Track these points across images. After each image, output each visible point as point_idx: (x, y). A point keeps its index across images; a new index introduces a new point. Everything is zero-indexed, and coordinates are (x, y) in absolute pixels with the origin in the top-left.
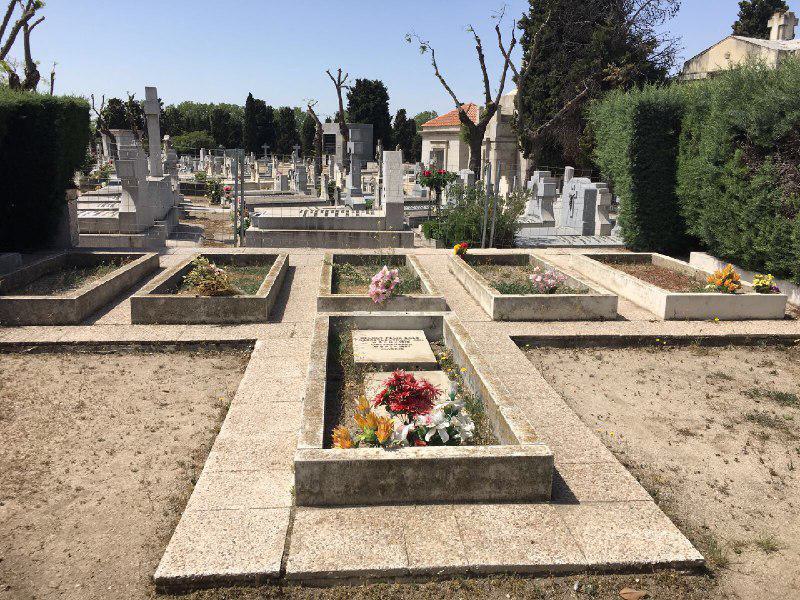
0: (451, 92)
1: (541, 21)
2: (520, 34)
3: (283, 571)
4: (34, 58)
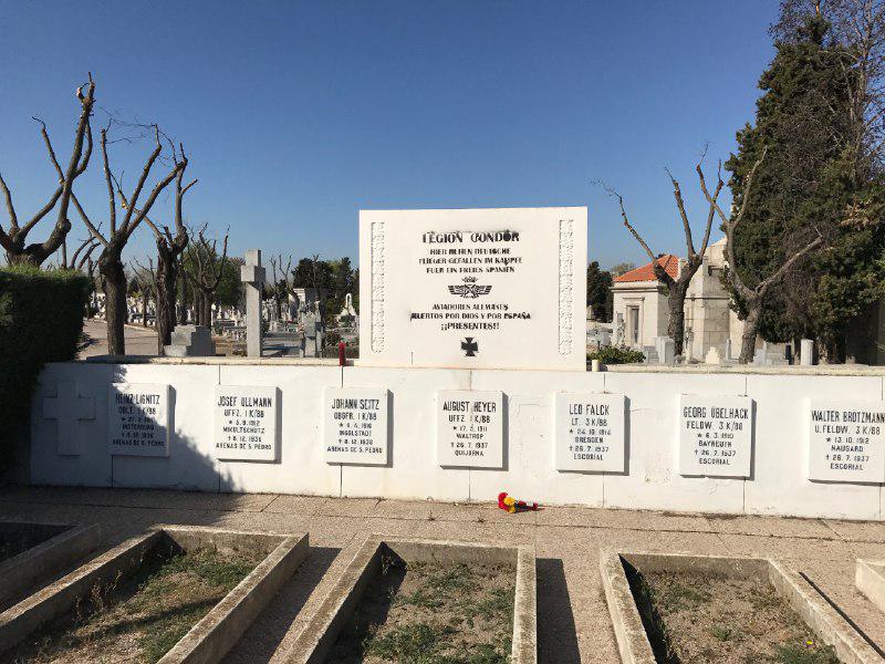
0: (643, 243)
1: (754, 159)
2: (728, 176)
3: (469, 499)
4: (95, 97)
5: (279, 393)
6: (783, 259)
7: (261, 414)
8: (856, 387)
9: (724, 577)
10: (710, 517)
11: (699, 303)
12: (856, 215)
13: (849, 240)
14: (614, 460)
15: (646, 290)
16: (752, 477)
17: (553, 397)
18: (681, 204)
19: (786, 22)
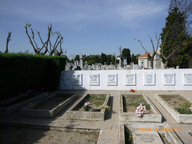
2: (160, 37)
5: (99, 74)
6: (172, 52)
7: (96, 78)
8: (188, 71)
9: (173, 97)
10: (169, 91)
11: (155, 61)
12: (185, 43)
13: (183, 49)
14: (153, 83)
15: (144, 59)
16: (175, 85)
17: (143, 74)
18: (152, 42)
19: (170, 8)
